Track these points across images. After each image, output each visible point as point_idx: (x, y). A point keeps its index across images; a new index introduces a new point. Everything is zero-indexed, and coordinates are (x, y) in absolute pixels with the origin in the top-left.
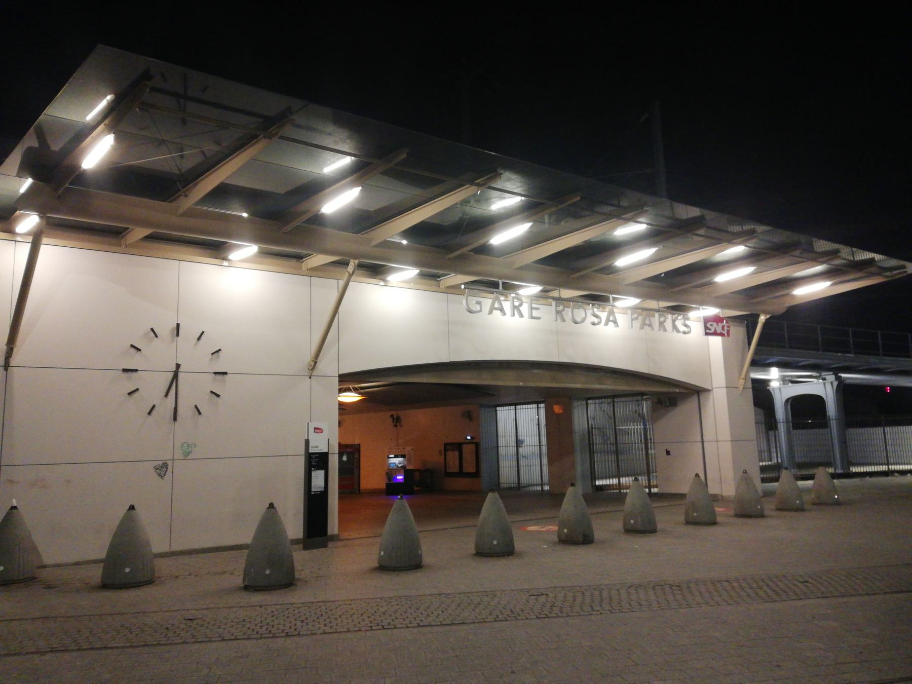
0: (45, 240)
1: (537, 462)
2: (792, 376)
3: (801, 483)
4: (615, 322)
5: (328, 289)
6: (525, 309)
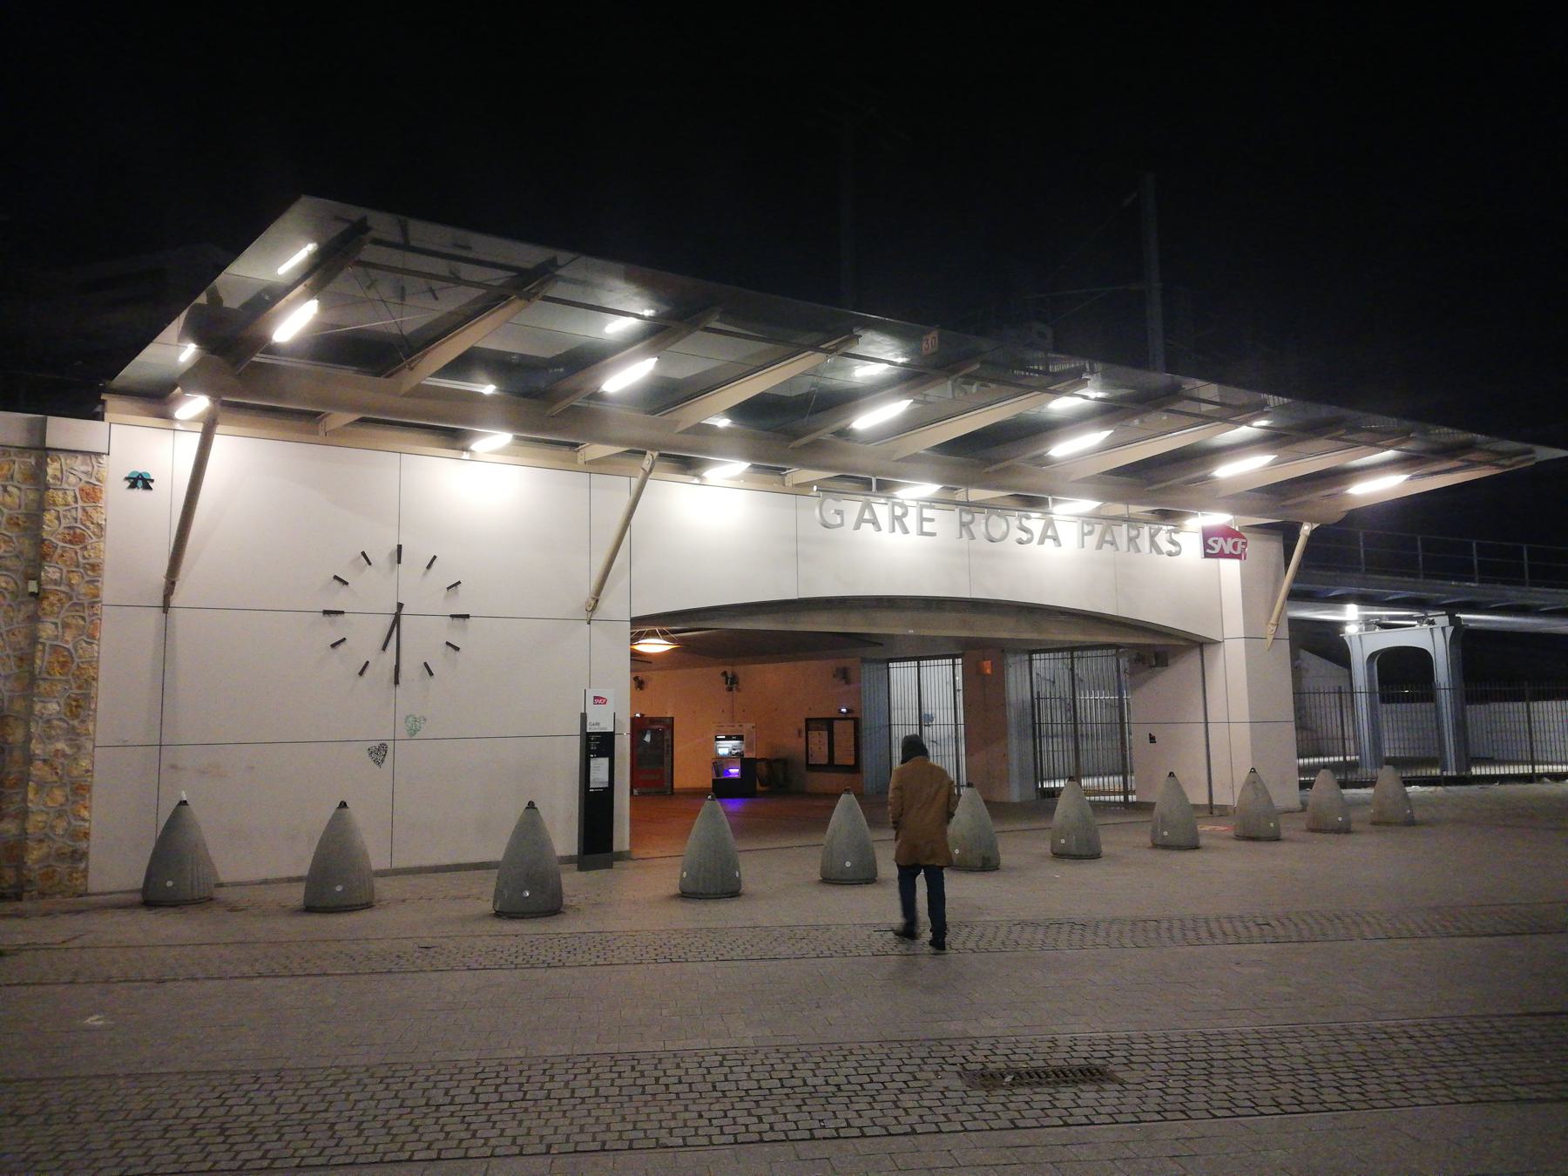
0: (219, 428)
1: (952, 750)
2: (1380, 617)
3: (1413, 790)
4: (1056, 539)
5: (614, 491)
6: (911, 521)
